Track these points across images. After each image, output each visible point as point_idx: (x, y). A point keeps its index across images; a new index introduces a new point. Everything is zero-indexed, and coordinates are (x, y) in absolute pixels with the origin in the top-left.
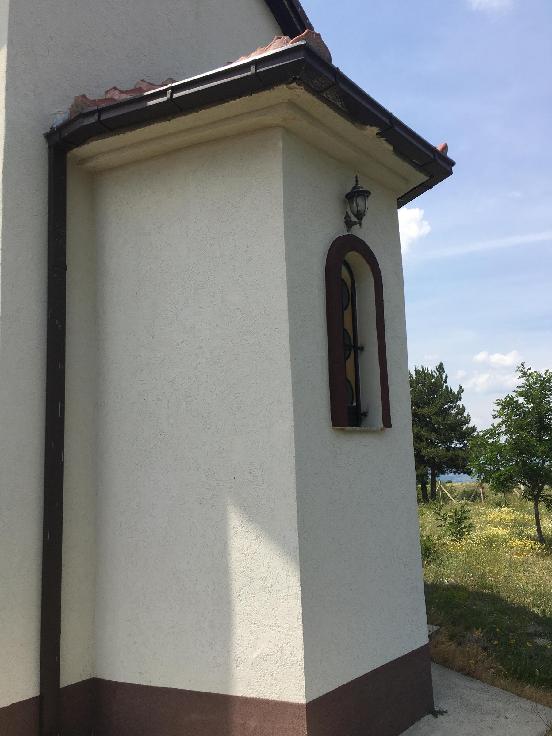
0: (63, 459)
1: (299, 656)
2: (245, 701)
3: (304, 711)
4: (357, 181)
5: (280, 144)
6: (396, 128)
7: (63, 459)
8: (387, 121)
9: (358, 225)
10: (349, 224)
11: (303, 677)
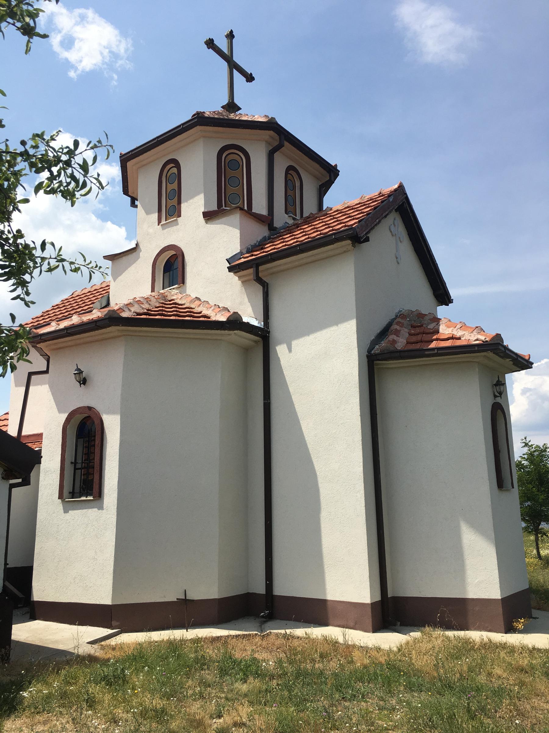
0: (82, 480)
1: (497, 580)
2: (473, 600)
3: (500, 602)
4: (498, 378)
5: (477, 369)
6: (311, 152)
7: (82, 480)
8: (514, 356)
9: (500, 398)
10: (495, 396)
11: (499, 588)
